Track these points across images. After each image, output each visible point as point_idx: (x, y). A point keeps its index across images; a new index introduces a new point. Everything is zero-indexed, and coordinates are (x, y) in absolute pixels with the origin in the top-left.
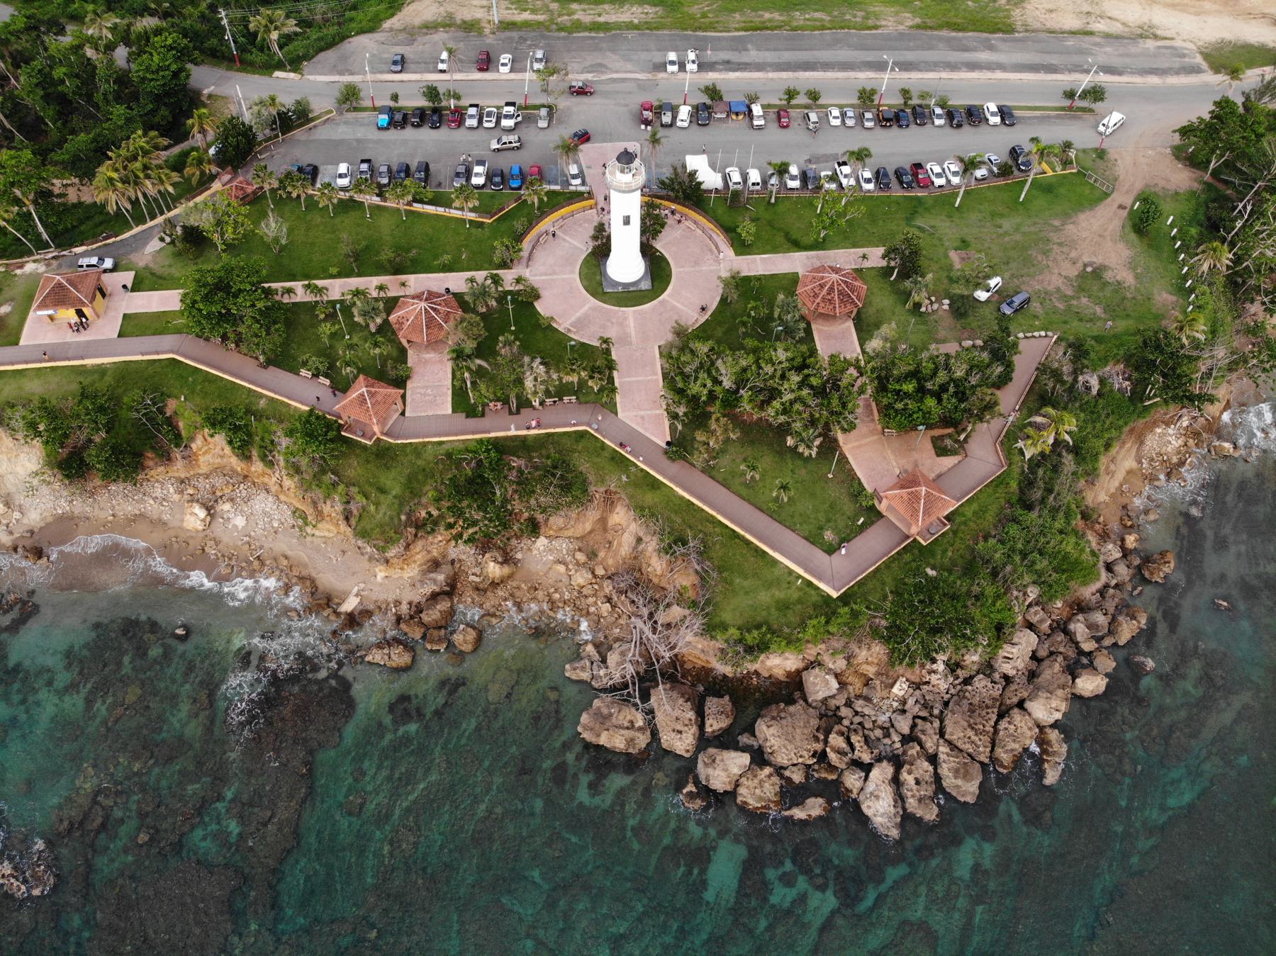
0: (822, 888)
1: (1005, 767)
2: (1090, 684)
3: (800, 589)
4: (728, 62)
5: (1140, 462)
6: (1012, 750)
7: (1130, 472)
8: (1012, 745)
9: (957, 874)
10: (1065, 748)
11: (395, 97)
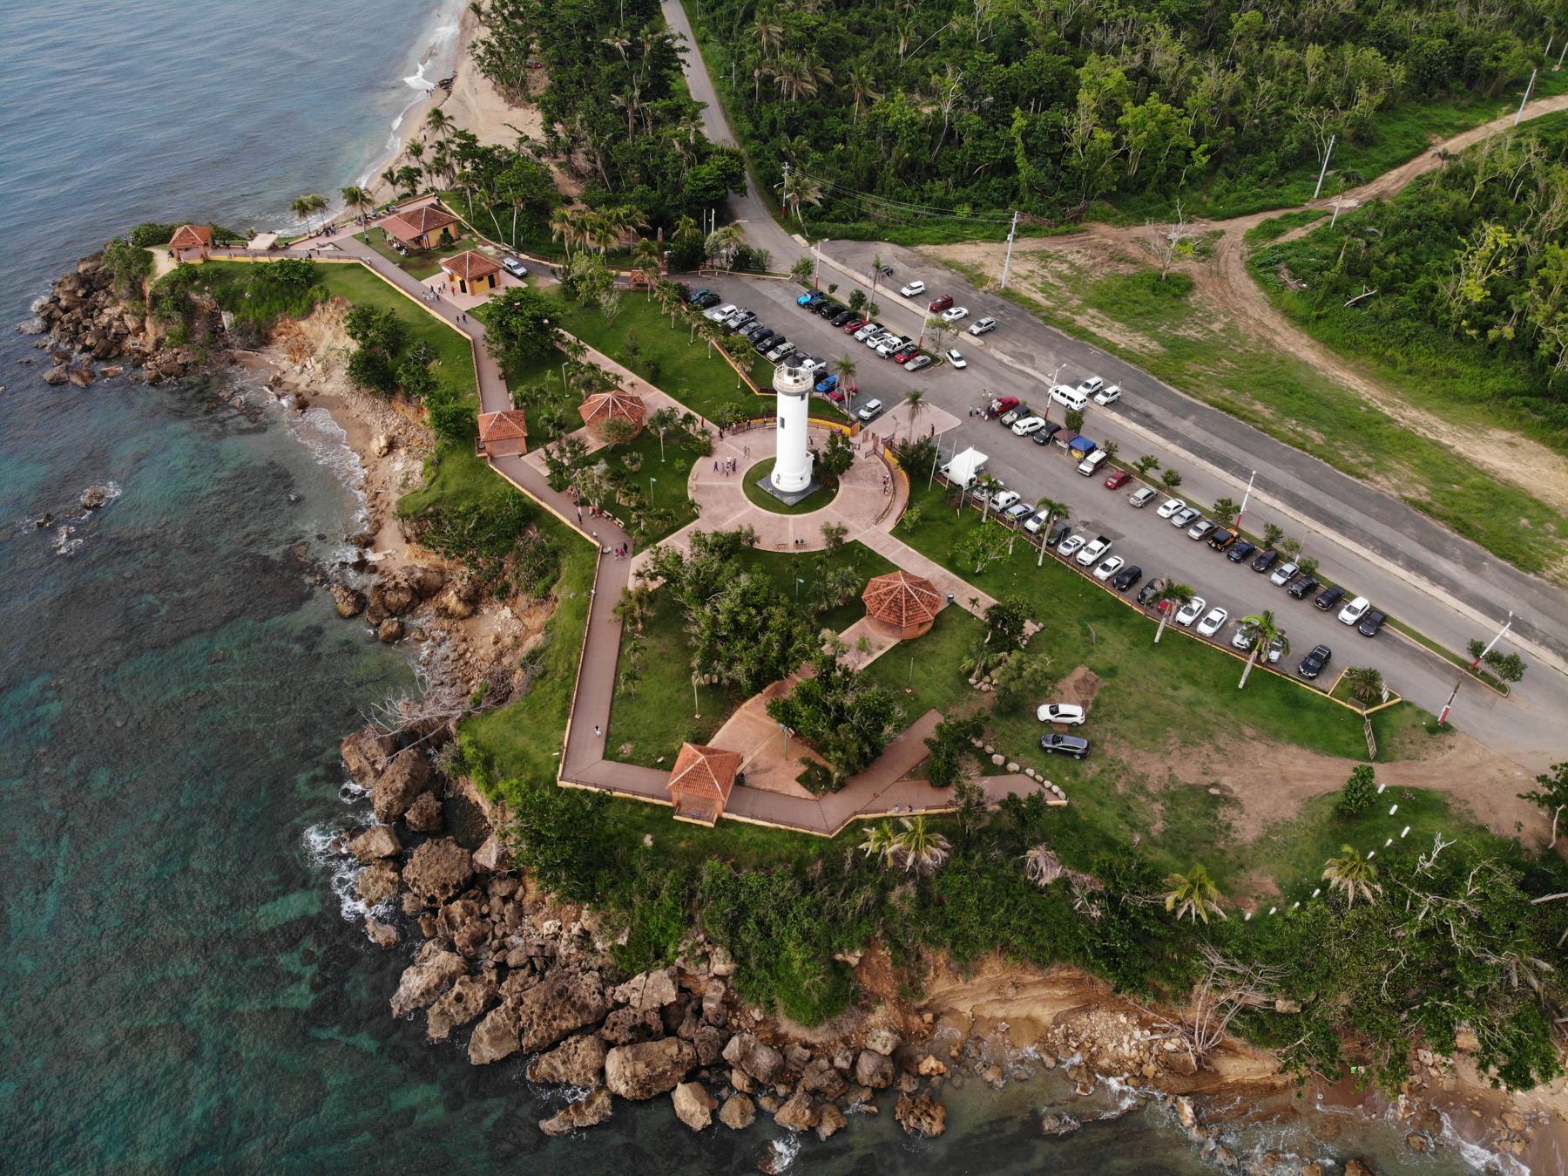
0: (315, 988)
1: (533, 1074)
2: (688, 1103)
3: (549, 759)
4: (1147, 416)
5: (1057, 1024)
6: (555, 1069)
7: (1032, 1021)
8: (557, 1063)
9: (393, 1096)
10: (594, 1120)
11: (833, 288)
